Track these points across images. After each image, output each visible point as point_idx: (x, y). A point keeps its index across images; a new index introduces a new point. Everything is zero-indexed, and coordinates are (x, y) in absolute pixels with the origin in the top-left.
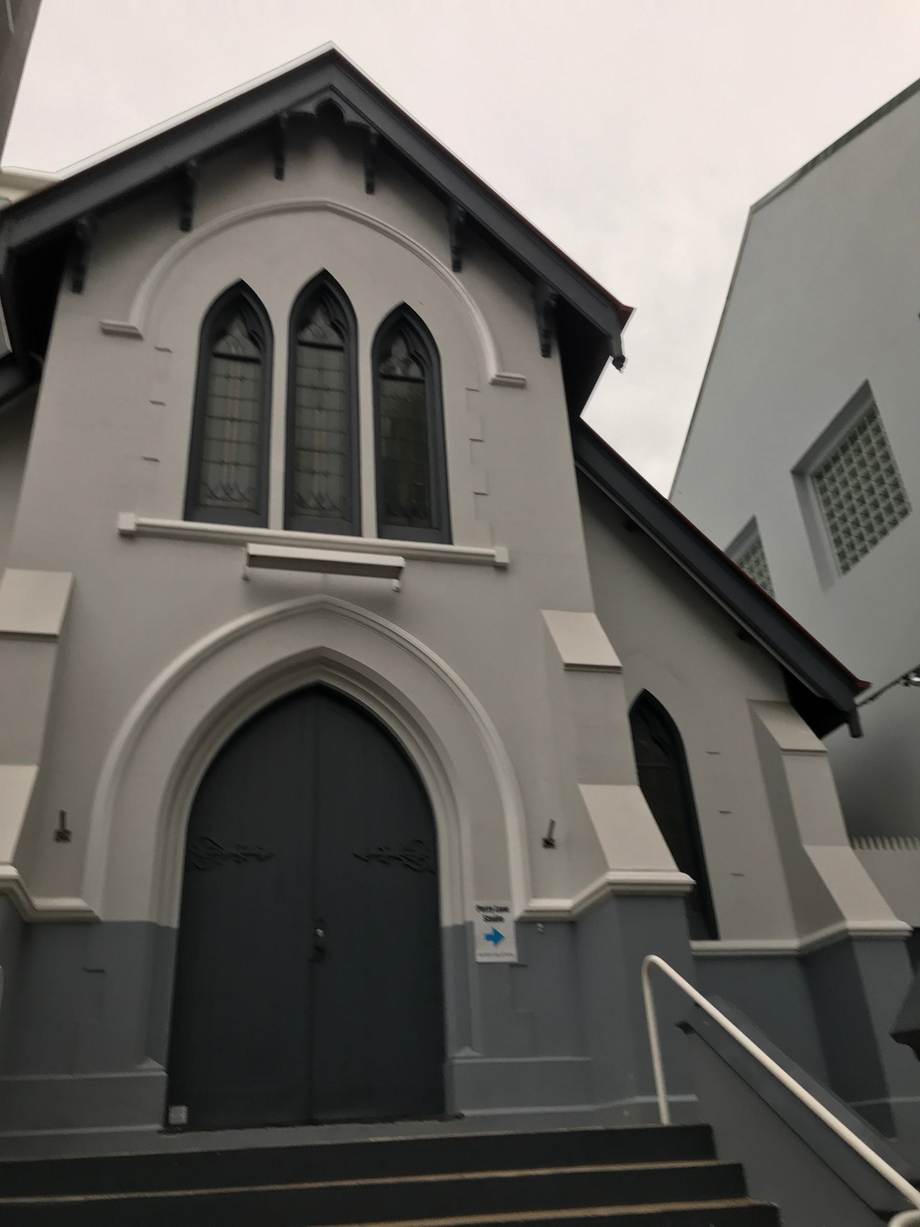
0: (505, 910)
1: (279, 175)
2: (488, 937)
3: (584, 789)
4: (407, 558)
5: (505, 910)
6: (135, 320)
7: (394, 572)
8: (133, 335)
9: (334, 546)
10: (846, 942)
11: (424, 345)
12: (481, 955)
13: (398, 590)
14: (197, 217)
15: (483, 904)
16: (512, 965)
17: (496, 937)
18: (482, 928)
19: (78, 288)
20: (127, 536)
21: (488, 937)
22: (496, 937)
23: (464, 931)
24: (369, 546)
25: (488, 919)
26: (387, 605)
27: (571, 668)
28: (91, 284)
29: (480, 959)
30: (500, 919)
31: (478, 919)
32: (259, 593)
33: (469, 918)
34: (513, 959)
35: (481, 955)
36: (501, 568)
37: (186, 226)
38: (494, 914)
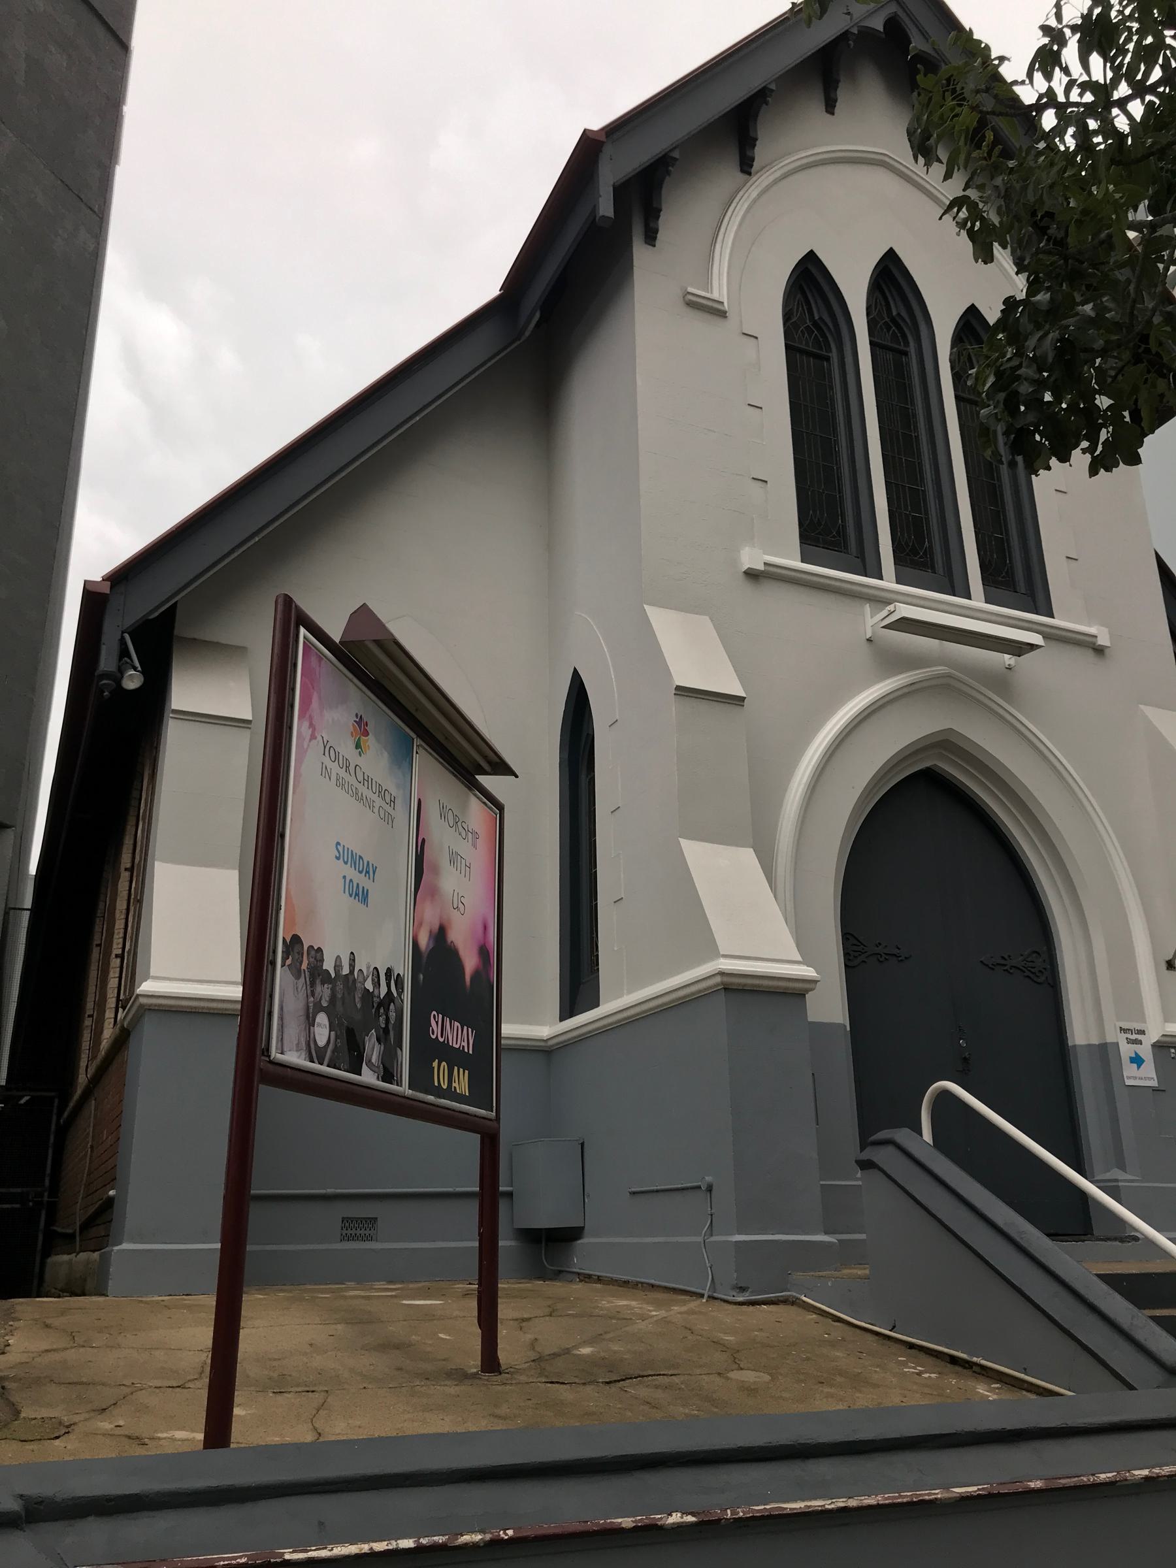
0: (1142, 1032)
1: (830, 107)
2: (1132, 1060)
3: (684, 842)
4: (1046, 637)
5: (1142, 1032)
6: (719, 291)
7: (1019, 649)
8: (716, 312)
9: (922, 603)
10: (1106, 1044)
11: (918, 339)
12: (1129, 1078)
13: (1009, 668)
14: (761, 153)
15: (1125, 1025)
16: (1154, 1090)
17: (1137, 1060)
18: (1126, 1051)
19: (651, 237)
20: (752, 575)
21: (1132, 1060)
22: (1137, 1060)
23: (1104, 1053)
24: (975, 611)
25: (1130, 1041)
26: (1002, 683)
27: (682, 691)
28: (664, 235)
29: (1128, 1082)
30: (1140, 1042)
31: (1122, 1039)
32: (890, 661)
33: (1110, 1039)
34: (1154, 1083)
35: (1129, 1078)
36: (1099, 651)
37: (746, 166)
38: (1135, 1035)
